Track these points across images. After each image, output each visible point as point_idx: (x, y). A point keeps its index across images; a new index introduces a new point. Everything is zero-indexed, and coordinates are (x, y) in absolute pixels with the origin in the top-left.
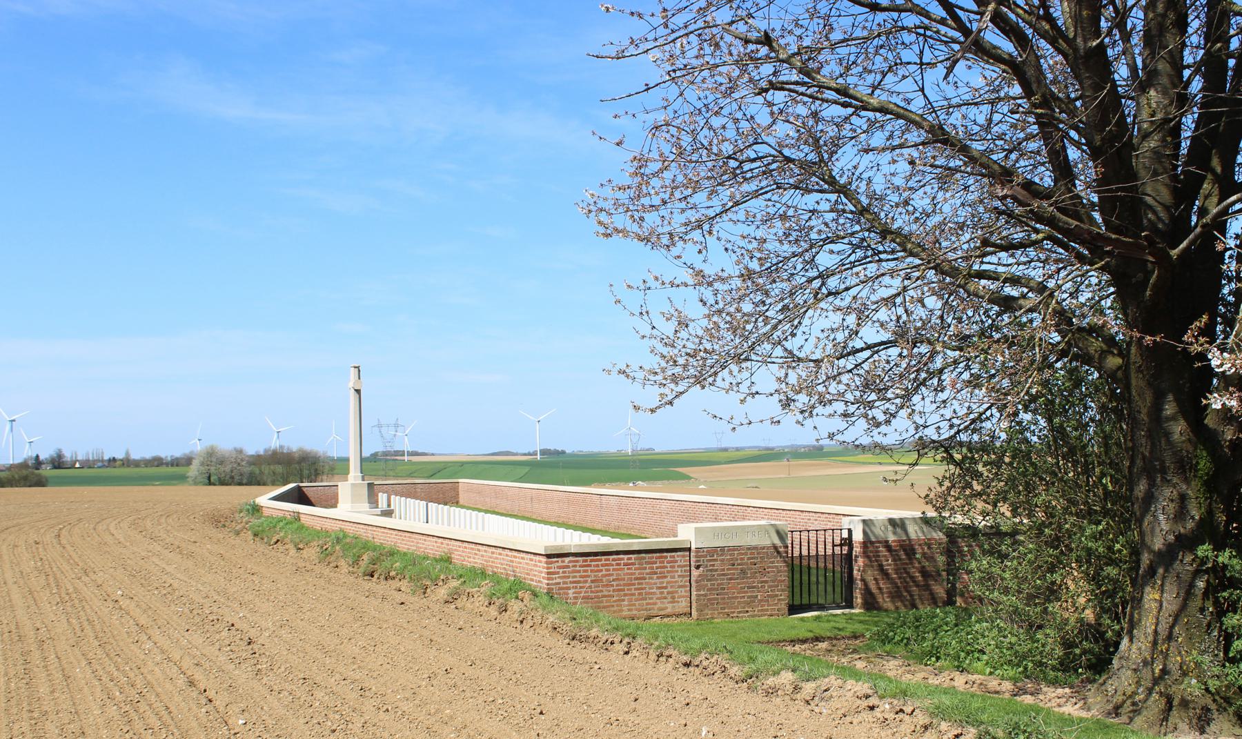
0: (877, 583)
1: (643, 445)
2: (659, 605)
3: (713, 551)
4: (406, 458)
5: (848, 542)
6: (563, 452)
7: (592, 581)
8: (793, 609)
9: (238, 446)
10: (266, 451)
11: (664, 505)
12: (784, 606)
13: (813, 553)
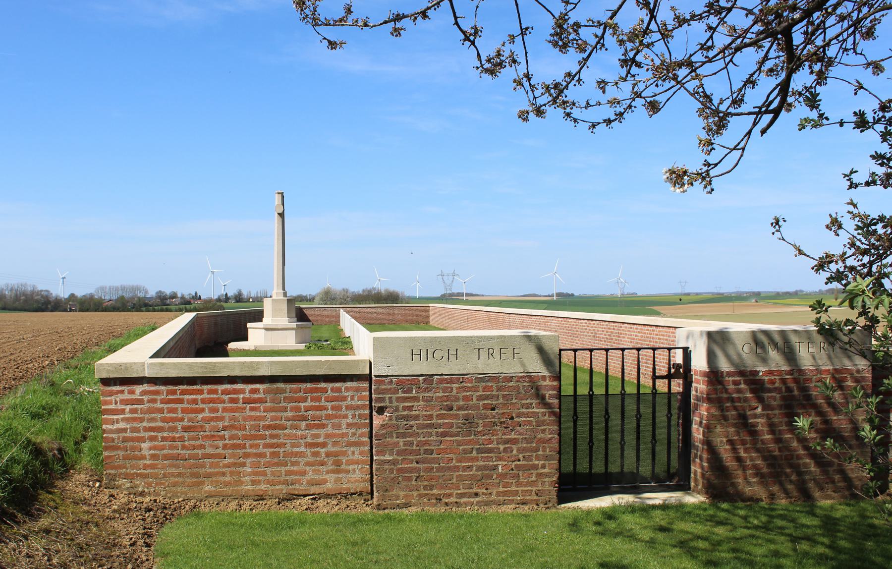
0: (734, 450)
1: (629, 290)
2: (311, 476)
3: (408, 382)
4: (464, 298)
5: (684, 372)
6: (573, 295)
7: (185, 429)
8: (572, 486)
9: (345, 287)
10: (363, 291)
11: (554, 320)
12: (549, 485)
13: (583, 390)
